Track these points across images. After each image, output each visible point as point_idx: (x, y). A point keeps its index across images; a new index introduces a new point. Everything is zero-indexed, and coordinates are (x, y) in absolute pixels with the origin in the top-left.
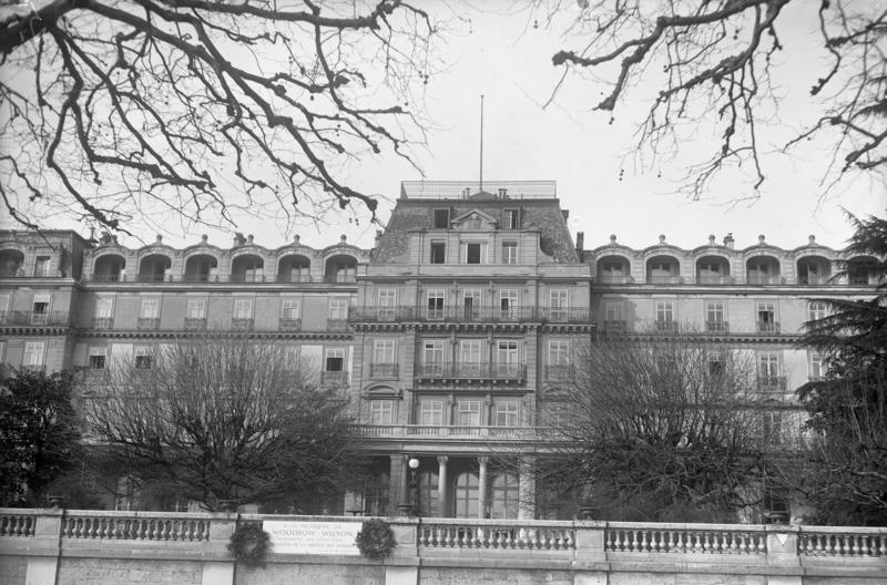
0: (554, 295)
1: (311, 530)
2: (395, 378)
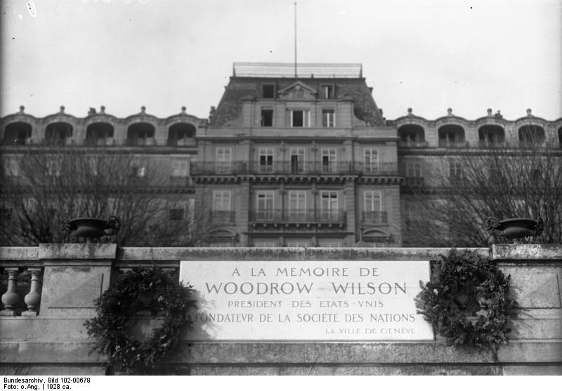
0: (368, 153)
1: (306, 280)
2: (232, 223)
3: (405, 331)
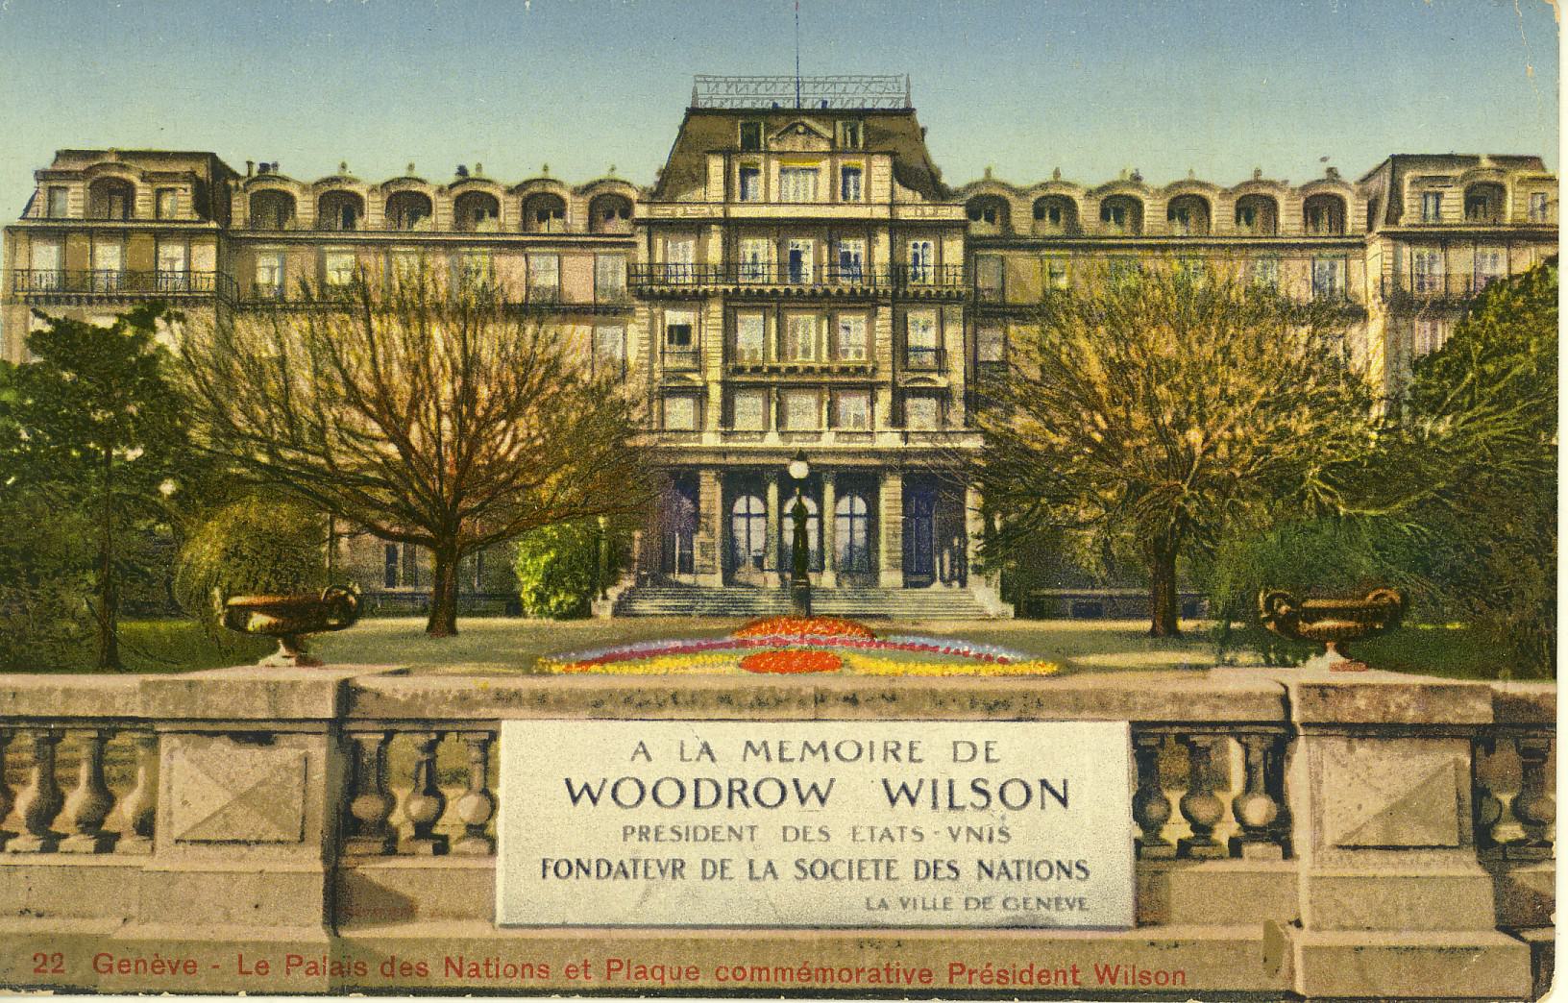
3: (1064, 904)
